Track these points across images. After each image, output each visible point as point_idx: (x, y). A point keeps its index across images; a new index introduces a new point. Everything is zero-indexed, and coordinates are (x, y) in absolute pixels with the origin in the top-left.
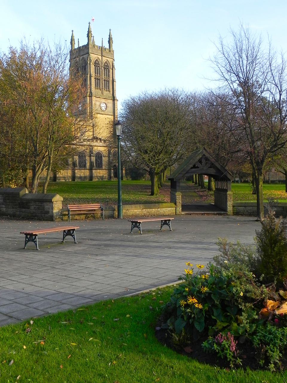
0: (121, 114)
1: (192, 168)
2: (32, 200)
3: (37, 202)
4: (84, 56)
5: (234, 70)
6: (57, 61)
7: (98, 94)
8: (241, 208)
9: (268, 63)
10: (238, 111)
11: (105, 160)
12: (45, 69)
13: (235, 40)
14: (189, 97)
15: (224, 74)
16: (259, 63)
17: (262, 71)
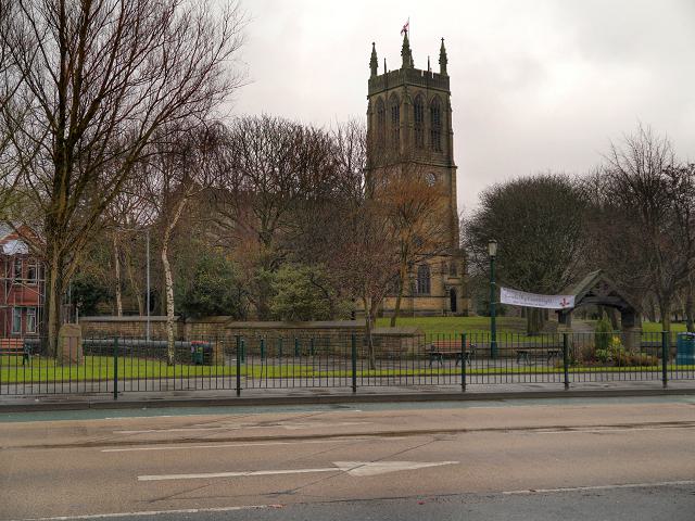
1: (587, 296)
4: (396, 90)
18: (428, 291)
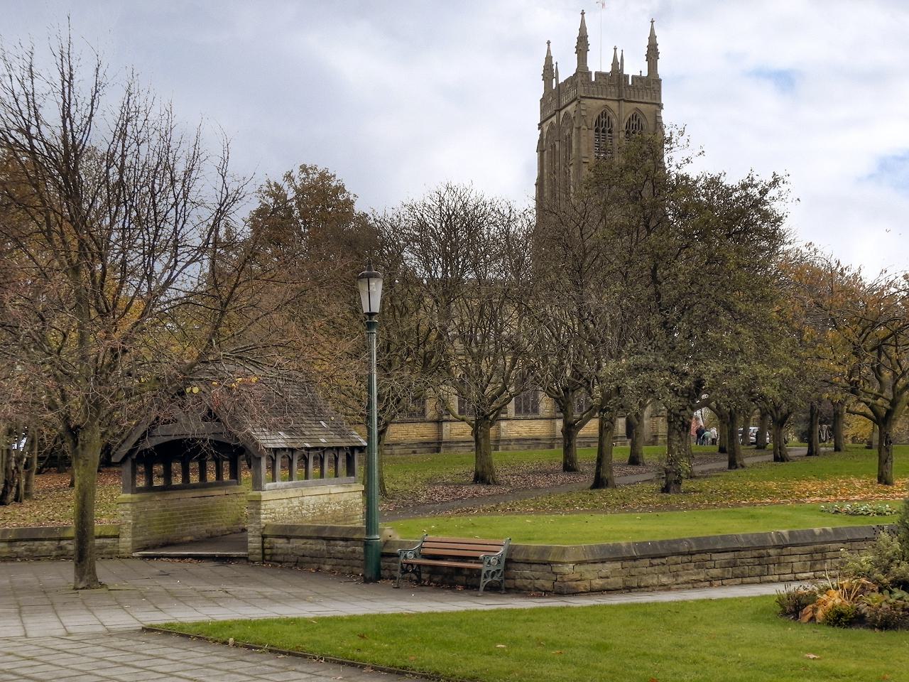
4: (569, 108)
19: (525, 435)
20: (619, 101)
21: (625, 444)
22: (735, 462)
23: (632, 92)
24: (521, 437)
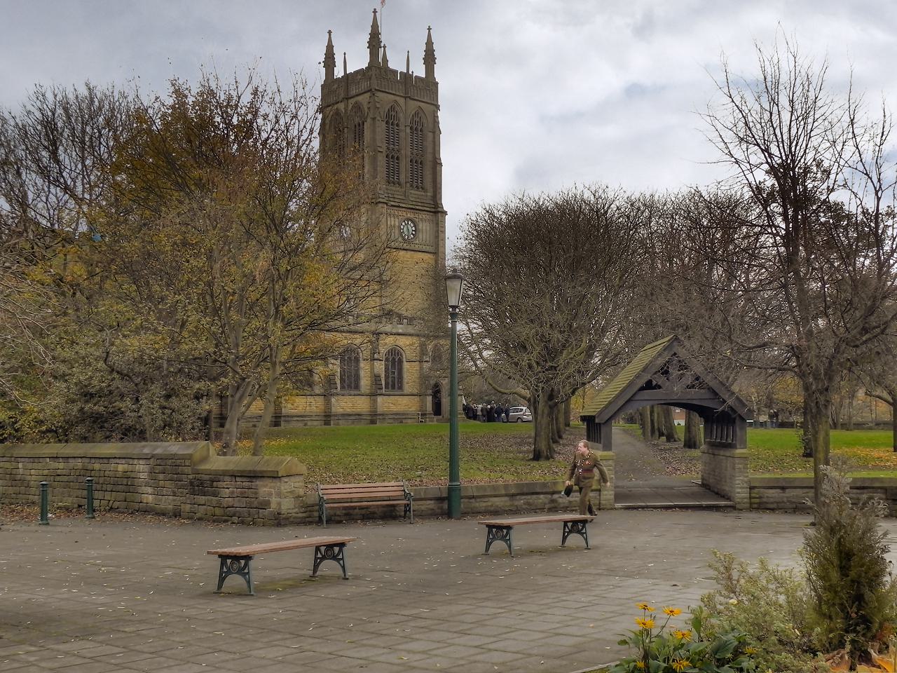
0: (458, 251)
1: (642, 389)
2: (225, 473)
3: (238, 479)
4: (360, 98)
5: (757, 137)
6: (295, 117)
7: (396, 196)
8: (773, 494)
9: (847, 119)
10: (765, 239)
11: (410, 372)
12: (264, 135)
13: (761, 60)
14: (637, 205)
15: (731, 146)
16: (824, 117)
17: (831, 138)
18: (401, 388)
19: (349, 410)
20: (405, 98)
21: (432, 421)
22: (673, 435)
23: (416, 91)
24: (345, 413)
